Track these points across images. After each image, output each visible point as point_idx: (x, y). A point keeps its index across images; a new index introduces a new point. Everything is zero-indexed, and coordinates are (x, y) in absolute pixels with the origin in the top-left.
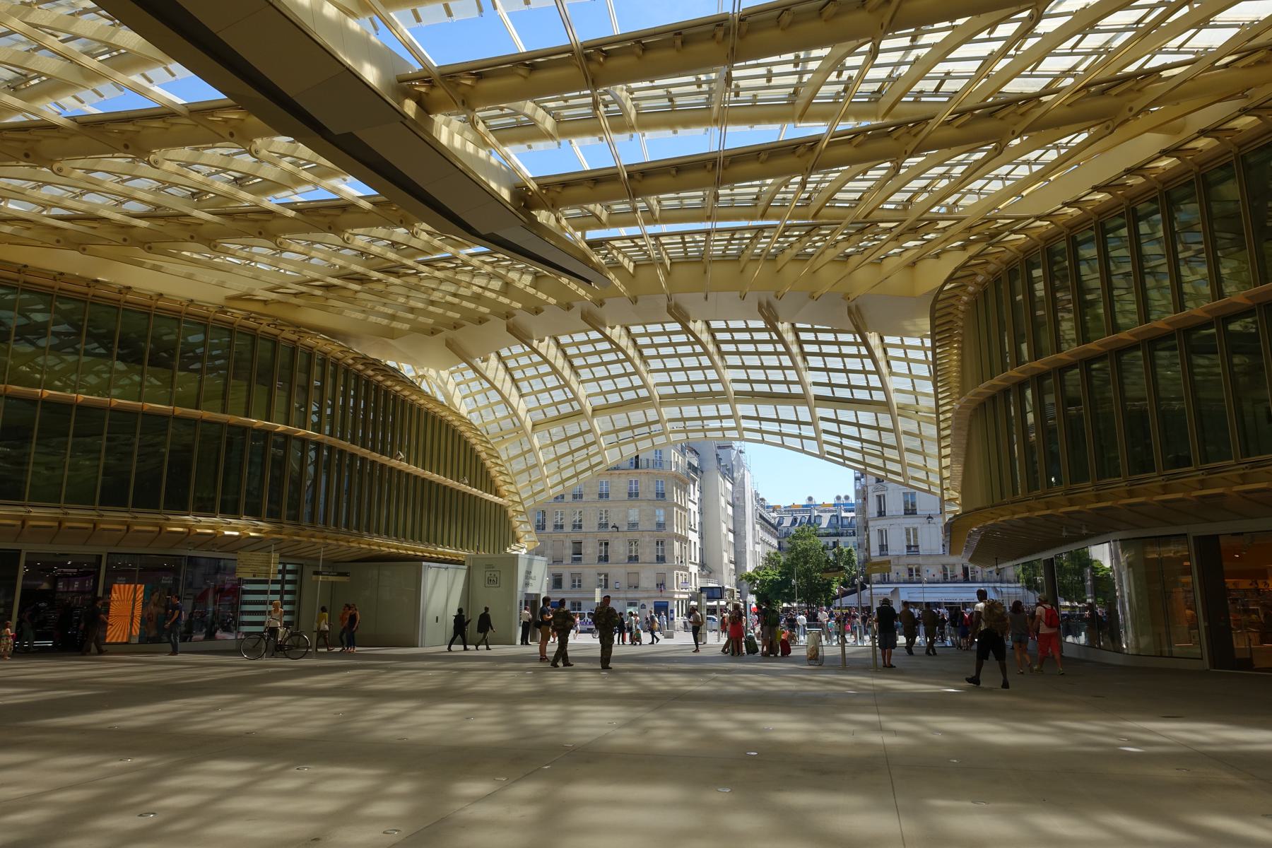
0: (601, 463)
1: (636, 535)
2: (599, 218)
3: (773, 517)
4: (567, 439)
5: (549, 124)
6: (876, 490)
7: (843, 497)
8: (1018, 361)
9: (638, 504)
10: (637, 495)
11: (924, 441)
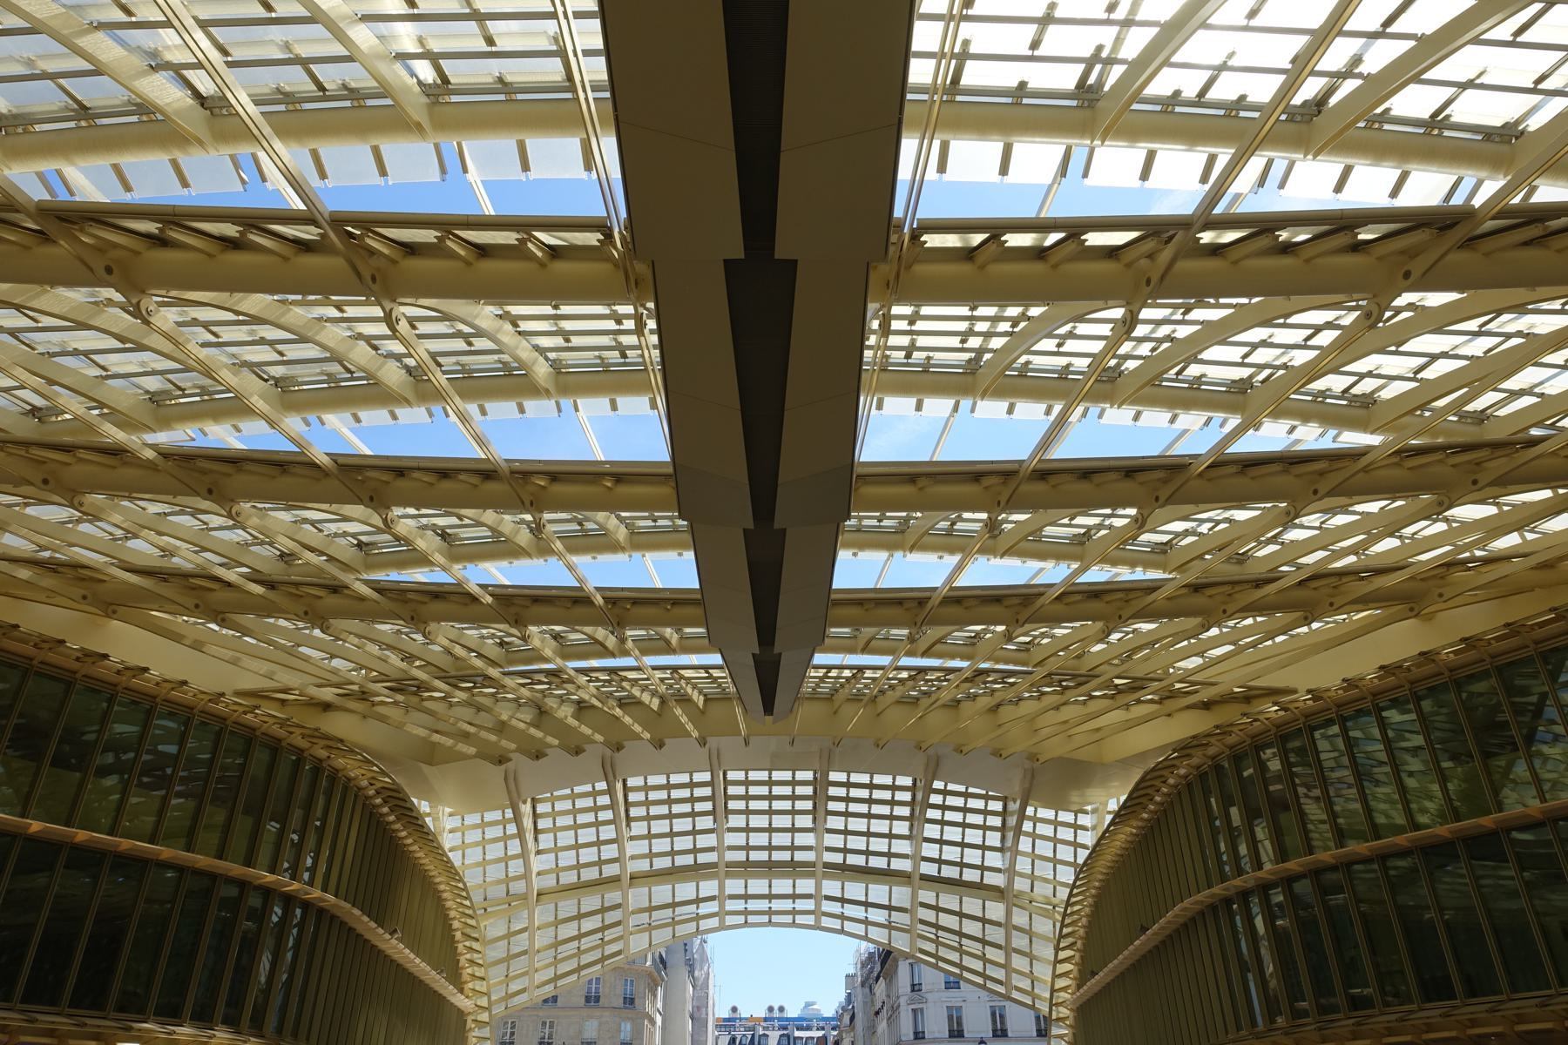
0: (619, 953)
2: (668, 642)
5: (622, 533)
6: (912, 1001)
7: (776, 1008)
9: (598, 1014)
10: (597, 999)
11: (1034, 939)
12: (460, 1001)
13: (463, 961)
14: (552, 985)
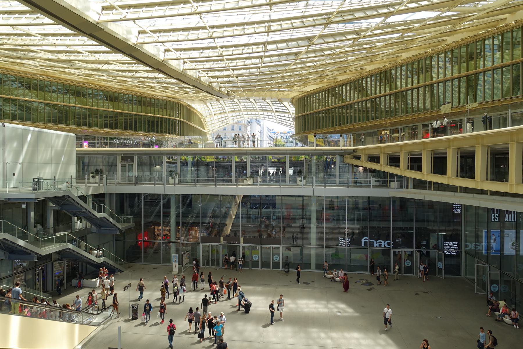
3: (274, 136)
4: (222, 118)
12: (204, 130)
13: (204, 125)
14: (514, 71)
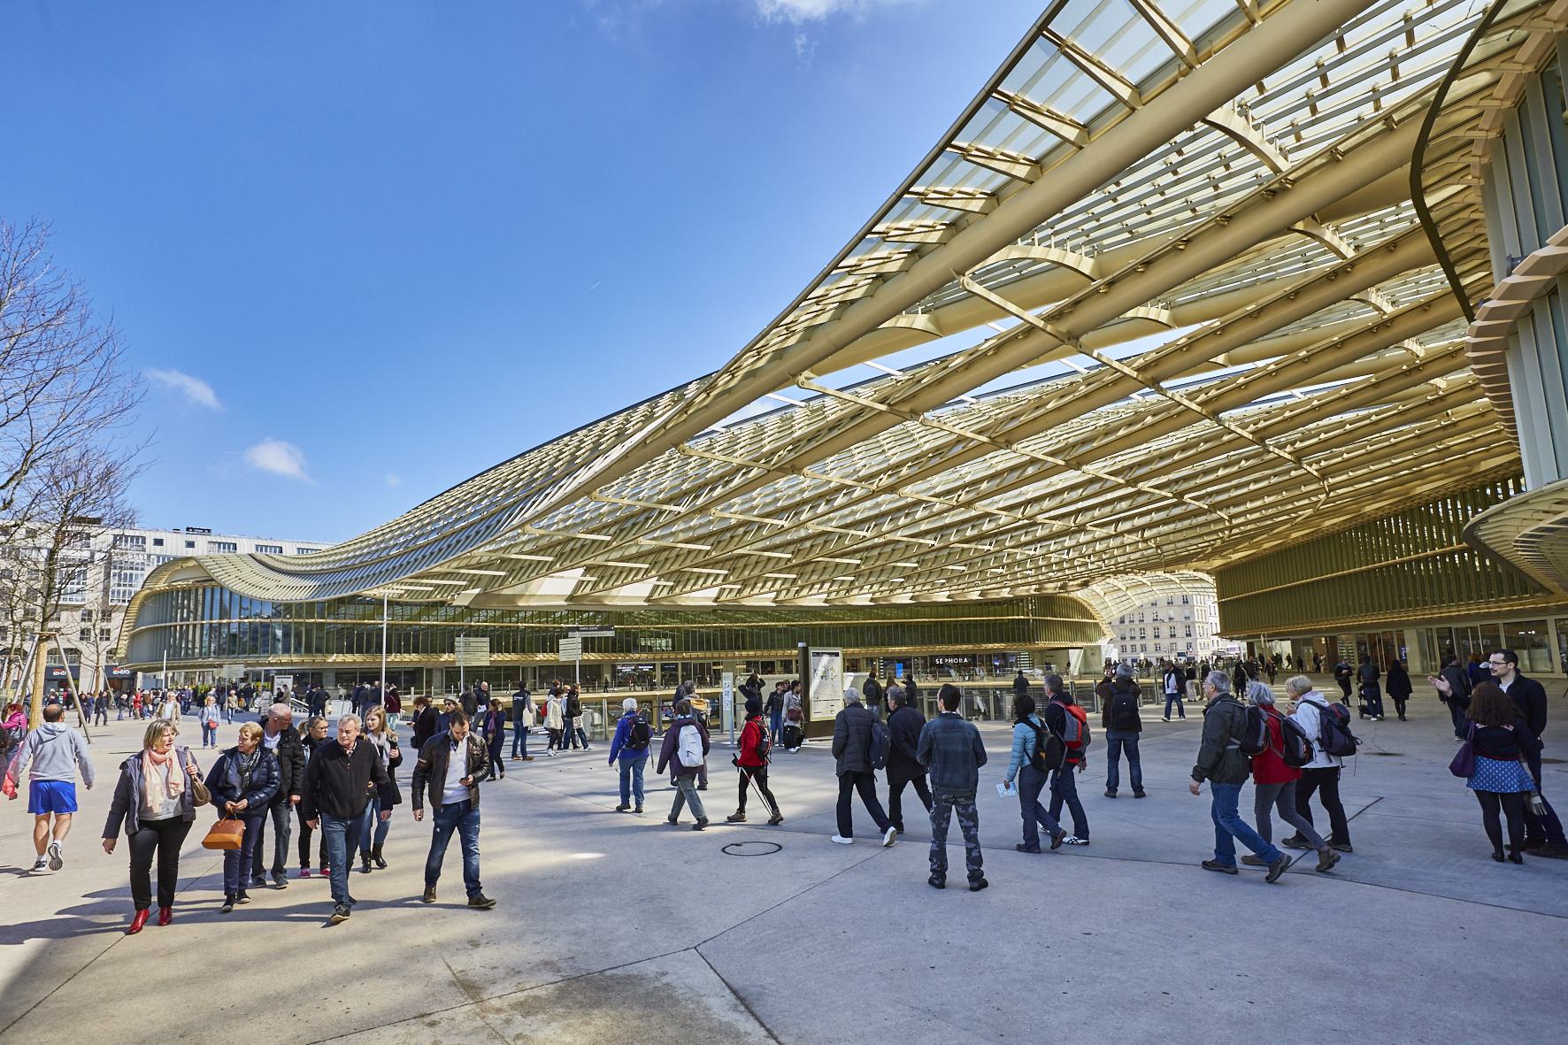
1: (1172, 624)
8: (1452, 544)
